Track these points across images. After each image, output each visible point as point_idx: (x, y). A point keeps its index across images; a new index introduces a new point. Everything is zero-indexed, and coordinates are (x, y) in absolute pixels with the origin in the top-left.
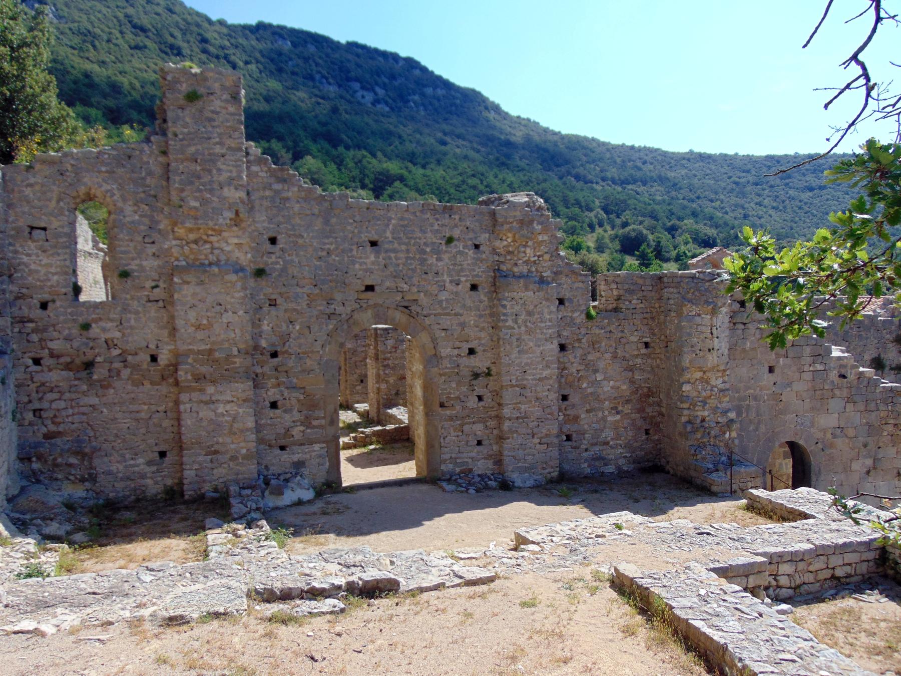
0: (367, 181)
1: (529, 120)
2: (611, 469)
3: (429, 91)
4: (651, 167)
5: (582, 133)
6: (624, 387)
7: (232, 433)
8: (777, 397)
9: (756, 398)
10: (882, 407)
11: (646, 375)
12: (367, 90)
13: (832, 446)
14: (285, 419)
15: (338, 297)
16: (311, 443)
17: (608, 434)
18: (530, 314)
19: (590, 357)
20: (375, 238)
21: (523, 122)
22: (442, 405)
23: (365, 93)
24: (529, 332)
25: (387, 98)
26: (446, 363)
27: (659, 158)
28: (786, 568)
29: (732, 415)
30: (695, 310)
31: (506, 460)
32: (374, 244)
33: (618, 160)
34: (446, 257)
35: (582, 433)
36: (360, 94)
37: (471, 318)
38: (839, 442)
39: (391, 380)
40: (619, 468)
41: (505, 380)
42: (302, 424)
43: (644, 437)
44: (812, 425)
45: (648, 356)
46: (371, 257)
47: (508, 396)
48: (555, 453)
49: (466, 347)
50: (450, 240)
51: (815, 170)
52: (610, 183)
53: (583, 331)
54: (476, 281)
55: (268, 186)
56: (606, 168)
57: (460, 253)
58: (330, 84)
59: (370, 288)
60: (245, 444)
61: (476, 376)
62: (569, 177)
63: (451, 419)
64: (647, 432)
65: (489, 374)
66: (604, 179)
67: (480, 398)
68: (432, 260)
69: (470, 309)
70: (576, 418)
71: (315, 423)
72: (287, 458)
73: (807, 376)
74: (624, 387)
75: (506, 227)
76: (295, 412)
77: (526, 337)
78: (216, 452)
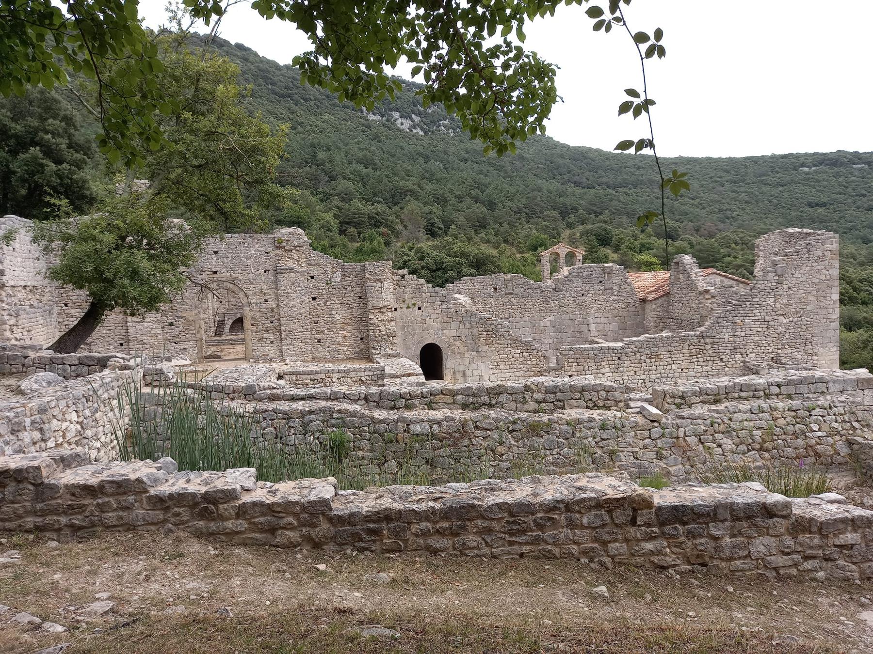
2: (342, 356)
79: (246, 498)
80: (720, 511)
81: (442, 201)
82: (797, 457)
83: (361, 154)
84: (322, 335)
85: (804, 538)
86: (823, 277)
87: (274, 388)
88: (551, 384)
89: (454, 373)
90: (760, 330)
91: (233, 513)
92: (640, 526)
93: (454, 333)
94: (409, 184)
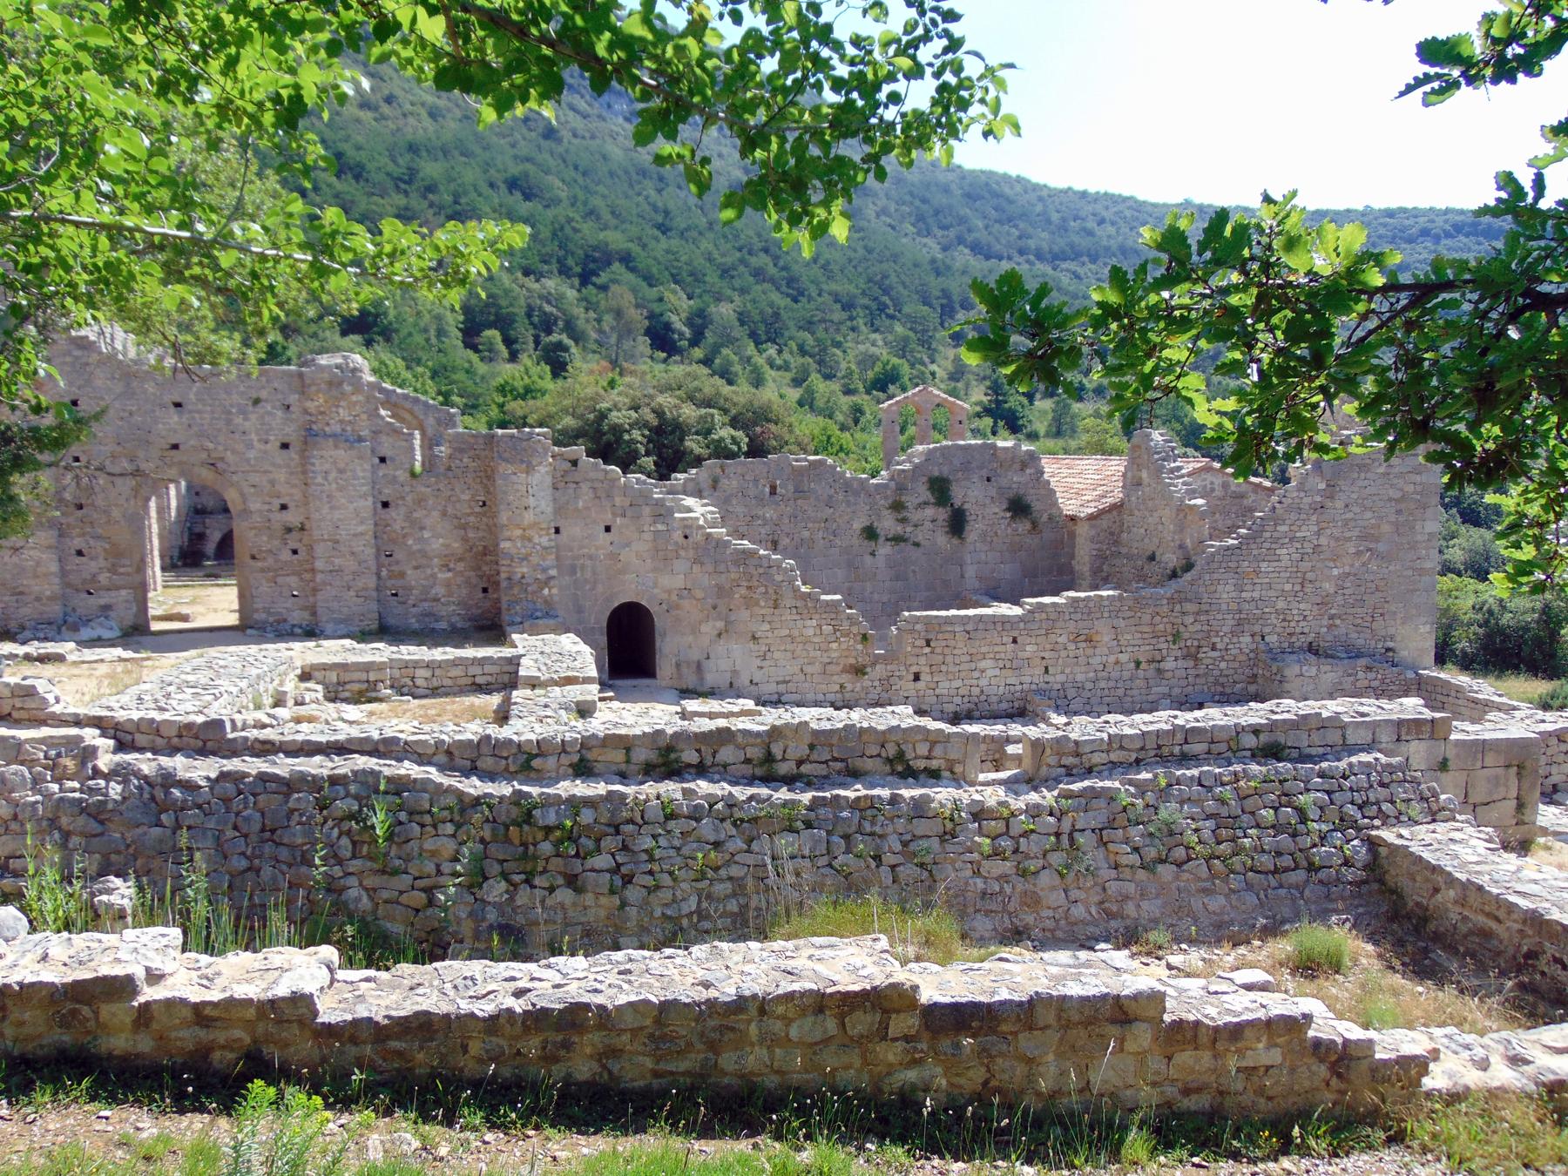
0: (570, 262)
2: (443, 625)
4: (1111, 230)
6: (456, 545)
7: (36, 577)
8: (614, 557)
9: (591, 557)
10: (732, 569)
11: (481, 534)
13: (678, 607)
14: (90, 566)
15: (141, 454)
16: (118, 588)
17: (439, 590)
18: (341, 471)
19: (415, 515)
20: (178, 400)
22: (253, 557)
24: (340, 489)
26: (257, 518)
27: (1128, 213)
28: (421, 673)
29: (553, 572)
30: (510, 469)
31: (320, 611)
32: (178, 405)
33: (1055, 217)
34: (253, 417)
35: (411, 589)
37: (281, 476)
38: (686, 603)
40: (453, 626)
41: (316, 534)
42: (109, 571)
43: (481, 595)
44: (656, 585)
45: (484, 514)
46: (174, 418)
47: (320, 550)
48: (374, 606)
49: (277, 503)
50: (257, 402)
51: (1394, 237)
52: (1032, 258)
53: (407, 489)
54: (286, 440)
55: (69, 353)
56: (1030, 230)
57: (270, 414)
59: (175, 447)
60: (50, 587)
61: (289, 530)
62: (961, 248)
63: (262, 570)
64: (485, 590)
65: (302, 529)
66: (1021, 252)
67: (295, 552)
68: (239, 420)
69: (280, 466)
70: (402, 575)
71: (122, 570)
72: (94, 602)
73: (648, 536)
74: (456, 545)
75: (314, 388)
76: (101, 560)
77: (338, 494)
78: (21, 593)
79: (149, 994)
80: (1039, 1010)
81: (688, 279)
82: (1275, 871)
83: (515, 170)
84: (400, 583)
85: (1185, 1057)
86: (1410, 488)
87: (264, 726)
88: (826, 726)
89: (678, 665)
90: (1288, 587)
91: (128, 1020)
92: (895, 1040)
93: (679, 582)
94: (616, 239)
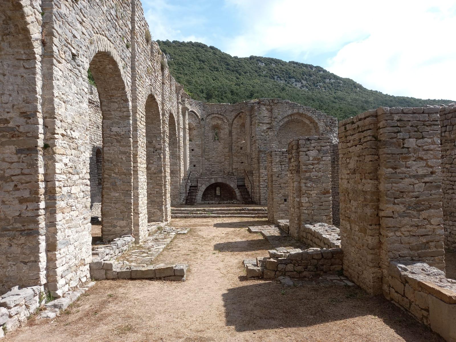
1: (377, 91)
3: (327, 81)
5: (405, 95)
12: (298, 82)
21: (374, 92)
23: (297, 83)
25: (307, 85)
36: (294, 84)
39: (314, 193)
58: (281, 80)
